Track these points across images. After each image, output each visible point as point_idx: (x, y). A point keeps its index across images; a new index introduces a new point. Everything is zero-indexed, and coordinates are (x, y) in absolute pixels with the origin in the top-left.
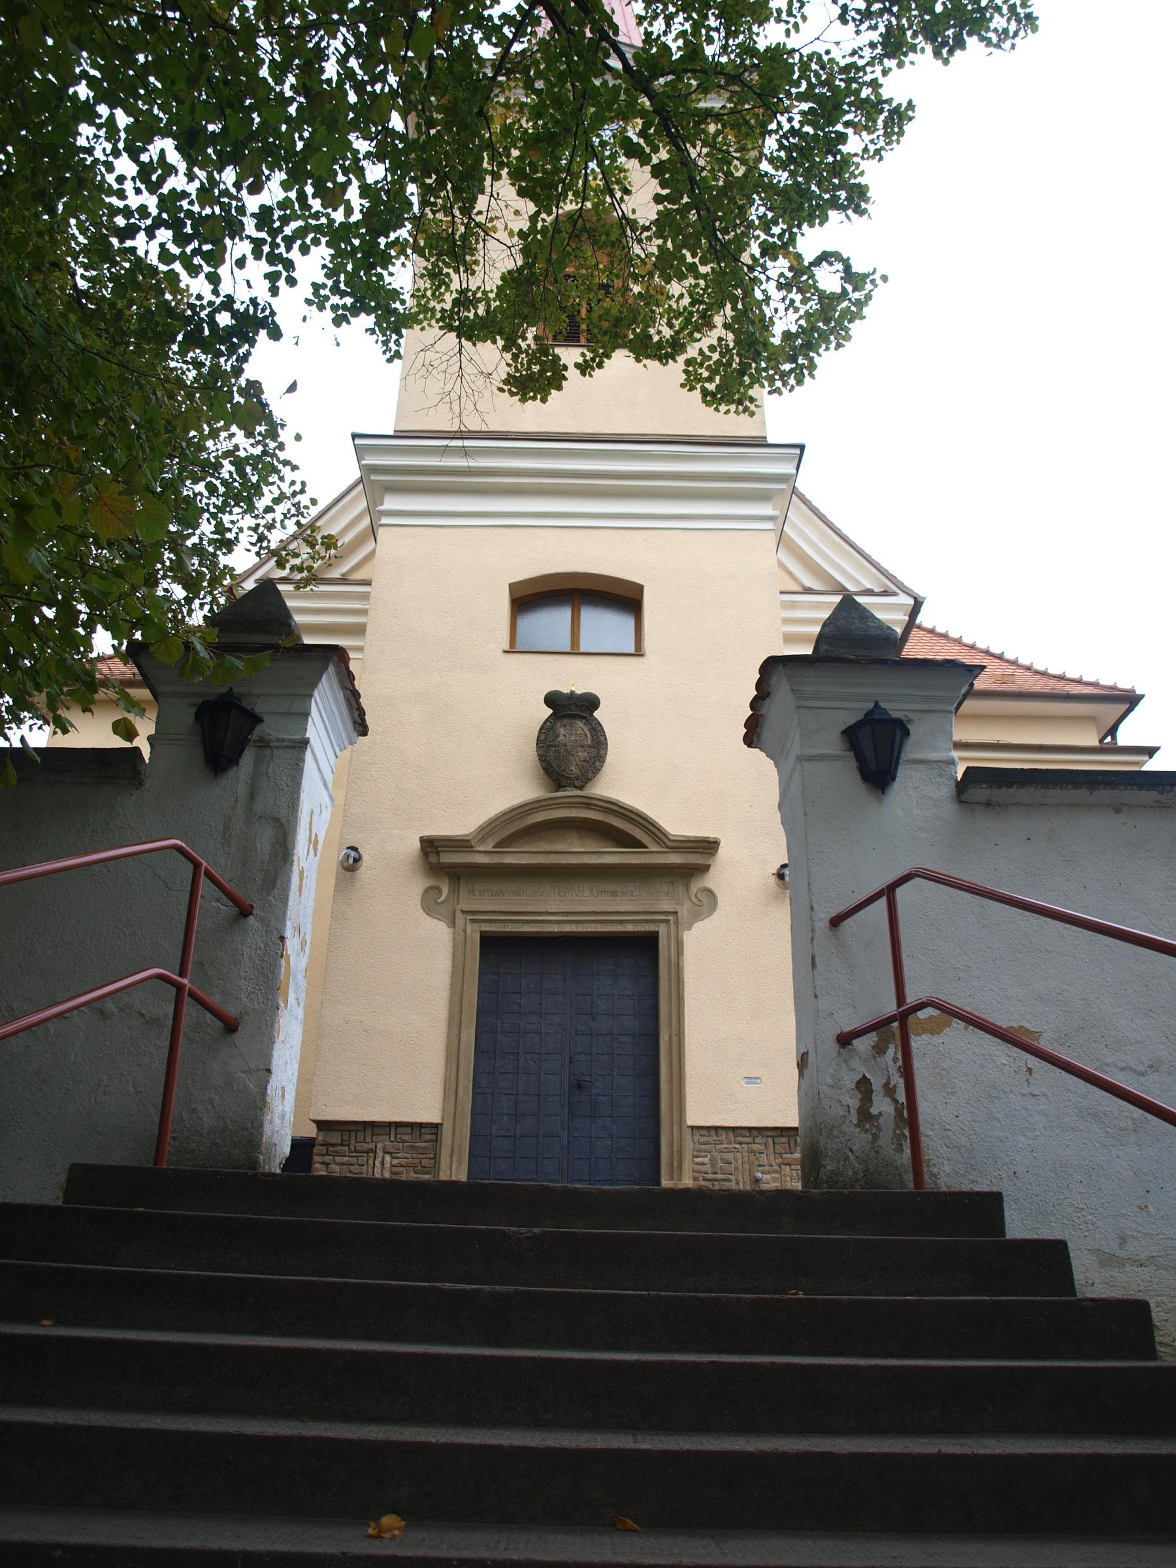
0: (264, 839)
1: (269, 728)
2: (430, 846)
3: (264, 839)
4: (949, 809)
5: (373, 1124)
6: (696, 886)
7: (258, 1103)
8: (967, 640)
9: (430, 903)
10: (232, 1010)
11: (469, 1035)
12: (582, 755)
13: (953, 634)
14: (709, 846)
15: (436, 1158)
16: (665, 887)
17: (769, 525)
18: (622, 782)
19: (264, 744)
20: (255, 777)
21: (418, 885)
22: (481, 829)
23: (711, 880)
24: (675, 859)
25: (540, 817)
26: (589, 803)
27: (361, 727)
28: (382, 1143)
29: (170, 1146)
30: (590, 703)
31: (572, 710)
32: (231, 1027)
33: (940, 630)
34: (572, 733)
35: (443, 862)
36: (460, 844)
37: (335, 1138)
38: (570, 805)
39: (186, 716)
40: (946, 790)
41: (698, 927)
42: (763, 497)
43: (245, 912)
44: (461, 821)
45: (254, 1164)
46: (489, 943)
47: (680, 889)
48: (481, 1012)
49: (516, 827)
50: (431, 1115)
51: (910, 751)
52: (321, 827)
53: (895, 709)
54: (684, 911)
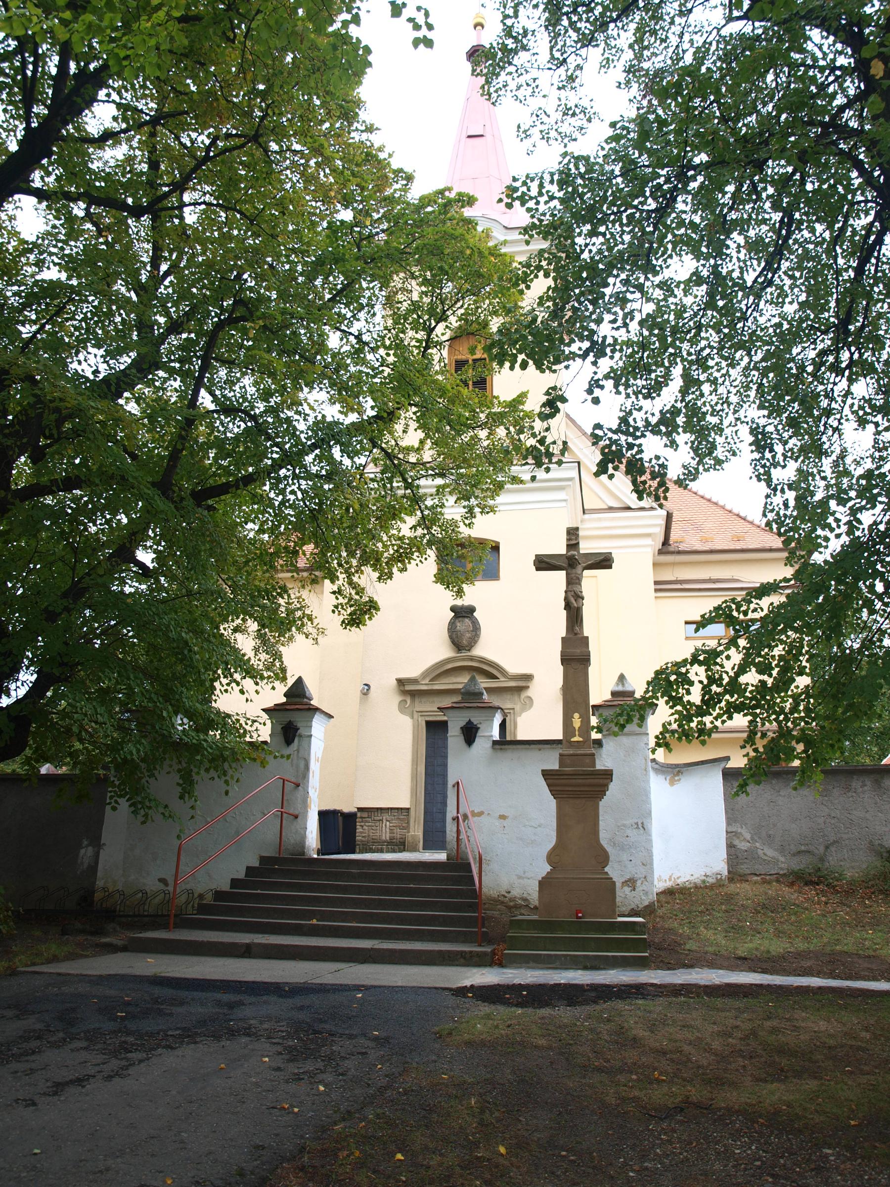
0: (302, 765)
1: (302, 731)
2: (401, 682)
3: (302, 765)
4: (490, 750)
5: (381, 809)
6: (524, 695)
7: (304, 837)
8: (728, 507)
9: (402, 708)
10: (296, 813)
11: (422, 769)
12: (468, 635)
13: (721, 503)
14: (528, 677)
15: (408, 823)
16: (509, 697)
17: (564, 504)
18: (487, 649)
19: (300, 736)
20: (299, 746)
21: (396, 699)
22: (423, 673)
23: (530, 693)
24: (512, 684)
25: (450, 666)
26: (472, 659)
27: (331, 717)
28: (385, 816)
29: (283, 848)
30: (471, 610)
31: (463, 613)
32: (296, 817)
33: (714, 500)
34: (463, 625)
35: (408, 690)
36: (414, 681)
37: (365, 815)
38: (464, 660)
39: (279, 728)
40: (490, 744)
41: (524, 715)
42: (561, 488)
43: (298, 785)
44: (413, 670)
45: (303, 853)
46: (429, 724)
47: (516, 698)
48: (427, 757)
49: (441, 671)
50: (405, 804)
51: (480, 733)
52: (320, 755)
53: (475, 721)
54: (518, 708)
